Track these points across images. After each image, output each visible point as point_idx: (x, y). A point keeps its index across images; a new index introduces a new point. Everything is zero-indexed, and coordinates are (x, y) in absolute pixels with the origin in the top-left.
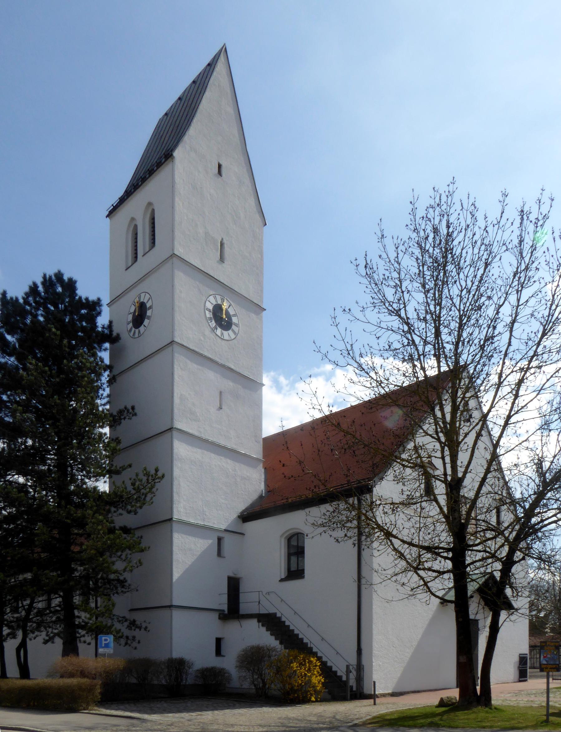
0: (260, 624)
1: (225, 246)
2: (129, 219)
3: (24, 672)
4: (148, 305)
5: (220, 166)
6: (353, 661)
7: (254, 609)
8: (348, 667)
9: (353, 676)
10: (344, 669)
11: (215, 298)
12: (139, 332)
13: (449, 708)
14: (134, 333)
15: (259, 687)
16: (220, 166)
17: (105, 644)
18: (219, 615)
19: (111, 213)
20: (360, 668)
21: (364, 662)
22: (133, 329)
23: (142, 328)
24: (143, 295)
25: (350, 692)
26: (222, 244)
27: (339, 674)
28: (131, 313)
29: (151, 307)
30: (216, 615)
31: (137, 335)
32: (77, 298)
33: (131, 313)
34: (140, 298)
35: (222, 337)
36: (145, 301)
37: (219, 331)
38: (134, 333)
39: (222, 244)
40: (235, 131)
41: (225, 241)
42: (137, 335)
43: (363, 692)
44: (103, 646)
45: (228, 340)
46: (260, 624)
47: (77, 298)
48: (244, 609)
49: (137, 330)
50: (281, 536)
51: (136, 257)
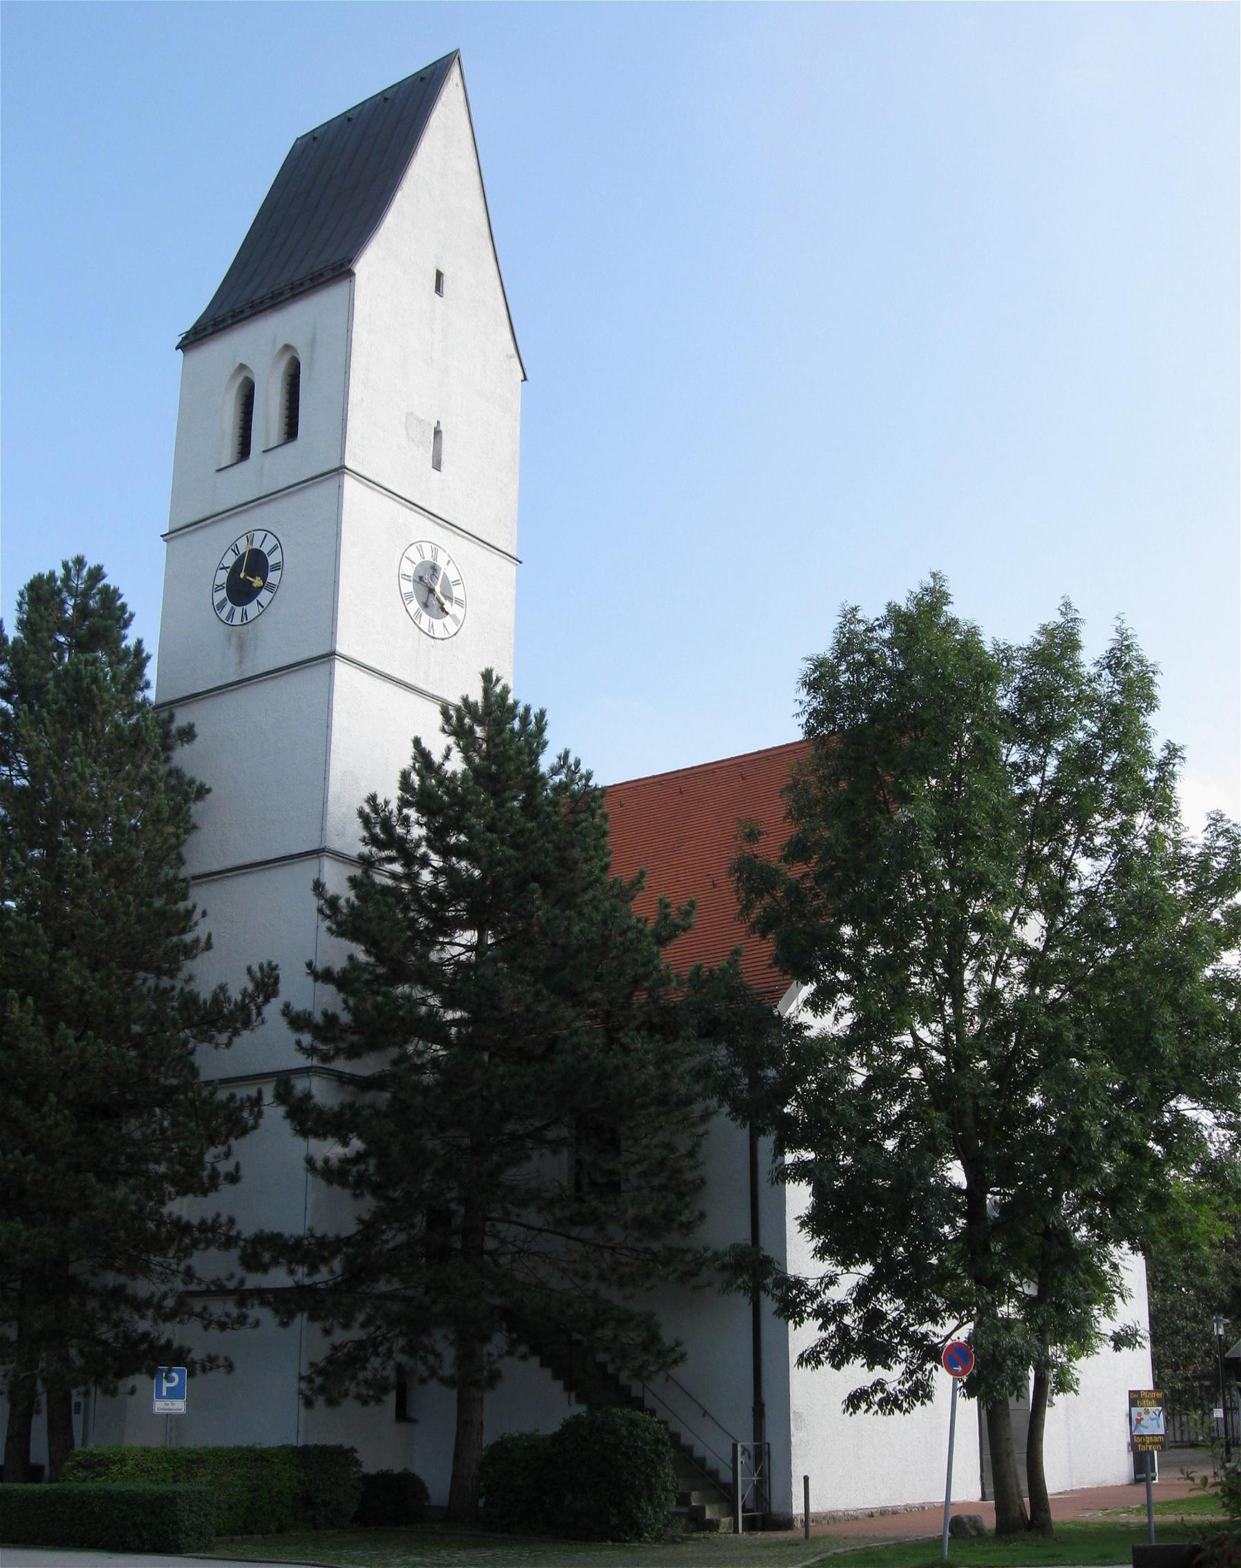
0: (573, 1395)
1: (444, 435)
2: (236, 366)
3: (84, 1444)
4: (272, 560)
5: (439, 275)
11: (420, 550)
12: (245, 614)
15: (659, 997)
16: (439, 275)
17: (168, 1389)
19: (193, 340)
22: (229, 605)
23: (252, 609)
24: (259, 536)
25: (743, 1512)
26: (437, 433)
28: (224, 568)
29: (277, 567)
31: (237, 620)
33: (224, 568)
34: (250, 541)
35: (431, 634)
36: (265, 550)
37: (425, 619)
39: (437, 433)
41: (442, 428)
42: (237, 620)
43: (770, 1513)
44: (164, 1394)
45: (443, 639)
46: (573, 1395)
49: (239, 610)
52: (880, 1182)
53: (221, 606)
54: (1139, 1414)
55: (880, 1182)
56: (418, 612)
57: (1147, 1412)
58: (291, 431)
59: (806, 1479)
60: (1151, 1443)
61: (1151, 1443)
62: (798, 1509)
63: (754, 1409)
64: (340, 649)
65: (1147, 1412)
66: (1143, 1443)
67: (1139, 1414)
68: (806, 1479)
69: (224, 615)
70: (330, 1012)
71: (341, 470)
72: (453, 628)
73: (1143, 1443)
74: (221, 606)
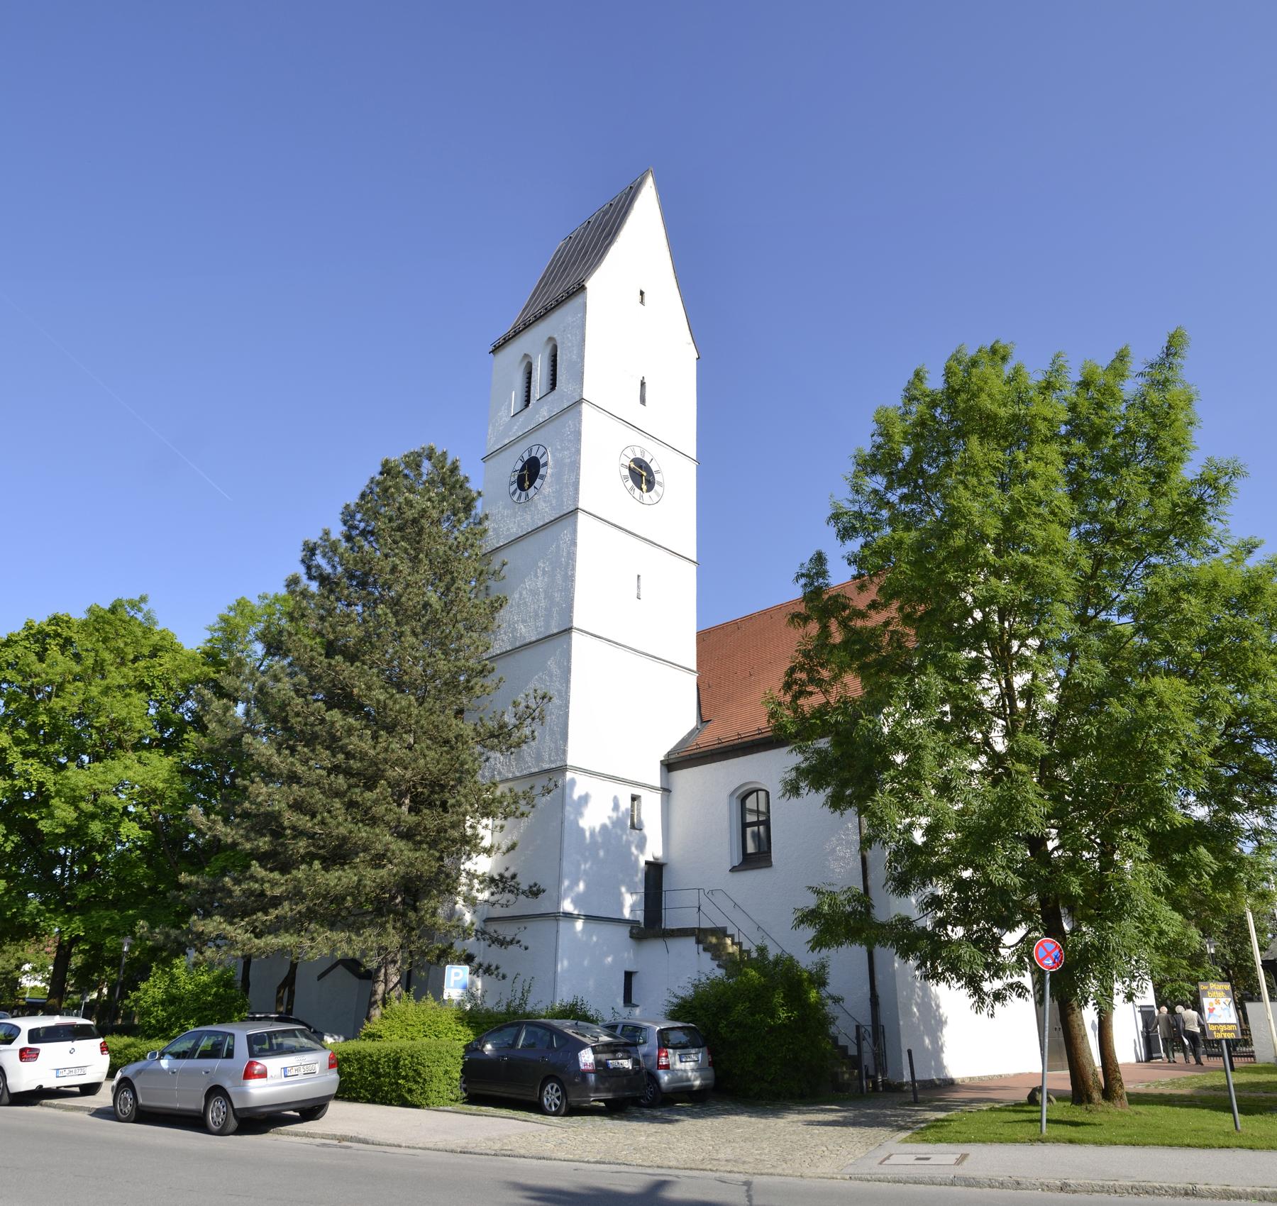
0: (701, 947)
1: (647, 385)
4: (542, 461)
6: (865, 1017)
7: (690, 920)
8: (858, 1027)
9: (867, 1046)
10: (853, 1034)
11: (633, 451)
13: (1100, 1070)
14: (520, 496)
18: (631, 932)
20: (878, 1030)
21: (883, 1020)
22: (518, 491)
24: (535, 449)
26: (643, 384)
27: (842, 1041)
30: (625, 931)
31: (523, 499)
32: (588, 834)
36: (538, 456)
38: (520, 496)
39: (643, 384)
40: (703, 712)
46: (701, 947)
47: (588, 834)
48: (671, 920)
50: (732, 794)
51: (528, 401)
52: (927, 1041)
53: (514, 493)
54: (1211, 1004)
55: (927, 1041)
56: (632, 487)
57: (1218, 1002)
58: (553, 384)
59: (910, 1052)
60: (1225, 1031)
61: (1225, 1031)
62: (907, 1077)
63: (871, 1000)
64: (581, 505)
65: (1218, 1002)
66: (1218, 1031)
67: (1211, 1004)
68: (910, 1052)
69: (515, 498)
70: (772, 953)
71: (581, 400)
72: (656, 499)
73: (1218, 1031)
74: (514, 493)
